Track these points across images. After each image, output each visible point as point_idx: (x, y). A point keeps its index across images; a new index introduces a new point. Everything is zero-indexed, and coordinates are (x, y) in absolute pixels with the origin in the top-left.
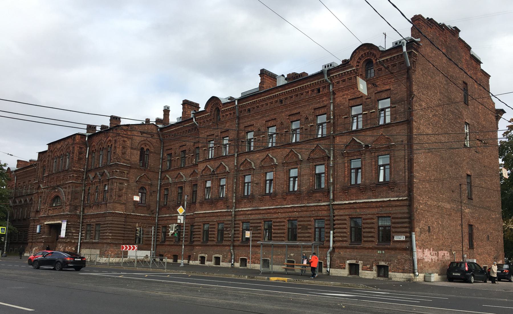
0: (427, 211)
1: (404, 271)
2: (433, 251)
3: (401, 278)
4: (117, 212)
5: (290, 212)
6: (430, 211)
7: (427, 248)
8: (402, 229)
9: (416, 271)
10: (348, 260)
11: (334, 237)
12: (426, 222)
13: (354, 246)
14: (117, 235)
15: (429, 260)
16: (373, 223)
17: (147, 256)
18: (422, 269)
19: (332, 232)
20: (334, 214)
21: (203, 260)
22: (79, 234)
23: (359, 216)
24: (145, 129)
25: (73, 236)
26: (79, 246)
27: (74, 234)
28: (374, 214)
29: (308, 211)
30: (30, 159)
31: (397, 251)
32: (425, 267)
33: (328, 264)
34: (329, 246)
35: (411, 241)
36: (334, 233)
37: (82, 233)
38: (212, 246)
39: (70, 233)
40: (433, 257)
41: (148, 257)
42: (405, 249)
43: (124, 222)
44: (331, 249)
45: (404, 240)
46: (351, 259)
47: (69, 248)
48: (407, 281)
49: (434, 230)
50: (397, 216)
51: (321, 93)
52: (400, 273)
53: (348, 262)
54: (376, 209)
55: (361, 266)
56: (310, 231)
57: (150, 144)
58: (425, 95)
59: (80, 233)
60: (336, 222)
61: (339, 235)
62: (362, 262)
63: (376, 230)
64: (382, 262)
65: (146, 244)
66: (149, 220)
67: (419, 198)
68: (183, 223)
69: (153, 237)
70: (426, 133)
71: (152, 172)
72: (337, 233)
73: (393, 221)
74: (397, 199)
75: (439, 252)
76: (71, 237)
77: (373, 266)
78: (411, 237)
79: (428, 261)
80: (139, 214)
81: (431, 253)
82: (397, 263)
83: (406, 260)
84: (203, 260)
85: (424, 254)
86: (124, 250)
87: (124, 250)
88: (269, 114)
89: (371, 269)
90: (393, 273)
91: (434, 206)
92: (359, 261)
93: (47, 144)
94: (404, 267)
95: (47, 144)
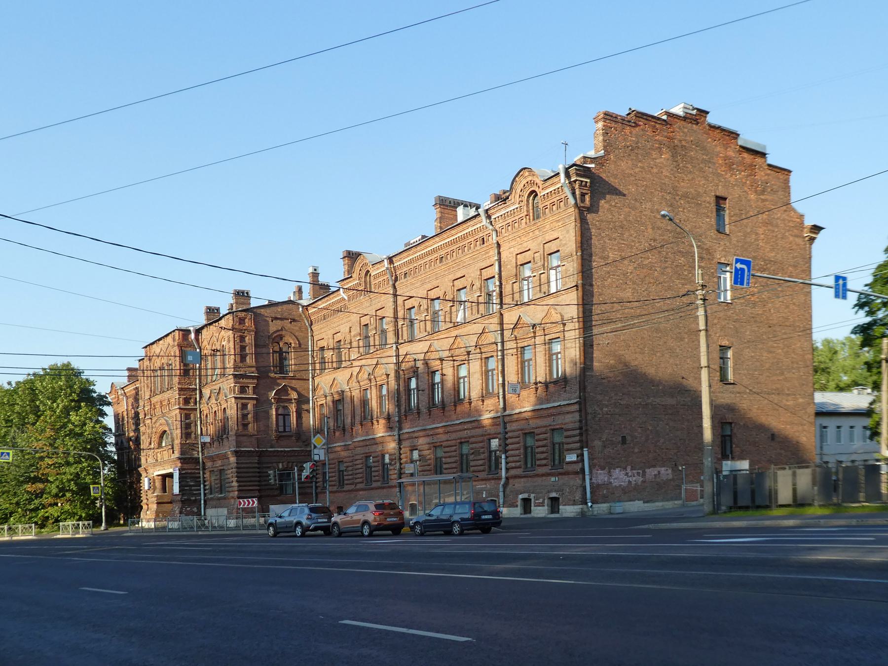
1: (574, 503)
4: (242, 449)
5: (460, 430)
9: (588, 501)
11: (507, 463)
14: (248, 484)
16: (545, 439)
18: (607, 497)
19: (503, 456)
25: (191, 490)
26: (202, 505)
27: (193, 488)
30: (604, 110)
33: (501, 501)
35: (583, 461)
36: (507, 457)
37: (205, 486)
38: (376, 489)
42: (577, 473)
43: (258, 463)
44: (503, 480)
47: (189, 509)
51: (485, 244)
53: (521, 496)
55: (533, 500)
56: (482, 456)
58: (615, 239)
59: (202, 486)
60: (509, 441)
68: (323, 459)
70: (617, 298)
72: (510, 456)
75: (648, 470)
76: (188, 492)
78: (582, 455)
80: (282, 449)
86: (241, 506)
87: (241, 506)
93: (143, 348)
95: (143, 348)
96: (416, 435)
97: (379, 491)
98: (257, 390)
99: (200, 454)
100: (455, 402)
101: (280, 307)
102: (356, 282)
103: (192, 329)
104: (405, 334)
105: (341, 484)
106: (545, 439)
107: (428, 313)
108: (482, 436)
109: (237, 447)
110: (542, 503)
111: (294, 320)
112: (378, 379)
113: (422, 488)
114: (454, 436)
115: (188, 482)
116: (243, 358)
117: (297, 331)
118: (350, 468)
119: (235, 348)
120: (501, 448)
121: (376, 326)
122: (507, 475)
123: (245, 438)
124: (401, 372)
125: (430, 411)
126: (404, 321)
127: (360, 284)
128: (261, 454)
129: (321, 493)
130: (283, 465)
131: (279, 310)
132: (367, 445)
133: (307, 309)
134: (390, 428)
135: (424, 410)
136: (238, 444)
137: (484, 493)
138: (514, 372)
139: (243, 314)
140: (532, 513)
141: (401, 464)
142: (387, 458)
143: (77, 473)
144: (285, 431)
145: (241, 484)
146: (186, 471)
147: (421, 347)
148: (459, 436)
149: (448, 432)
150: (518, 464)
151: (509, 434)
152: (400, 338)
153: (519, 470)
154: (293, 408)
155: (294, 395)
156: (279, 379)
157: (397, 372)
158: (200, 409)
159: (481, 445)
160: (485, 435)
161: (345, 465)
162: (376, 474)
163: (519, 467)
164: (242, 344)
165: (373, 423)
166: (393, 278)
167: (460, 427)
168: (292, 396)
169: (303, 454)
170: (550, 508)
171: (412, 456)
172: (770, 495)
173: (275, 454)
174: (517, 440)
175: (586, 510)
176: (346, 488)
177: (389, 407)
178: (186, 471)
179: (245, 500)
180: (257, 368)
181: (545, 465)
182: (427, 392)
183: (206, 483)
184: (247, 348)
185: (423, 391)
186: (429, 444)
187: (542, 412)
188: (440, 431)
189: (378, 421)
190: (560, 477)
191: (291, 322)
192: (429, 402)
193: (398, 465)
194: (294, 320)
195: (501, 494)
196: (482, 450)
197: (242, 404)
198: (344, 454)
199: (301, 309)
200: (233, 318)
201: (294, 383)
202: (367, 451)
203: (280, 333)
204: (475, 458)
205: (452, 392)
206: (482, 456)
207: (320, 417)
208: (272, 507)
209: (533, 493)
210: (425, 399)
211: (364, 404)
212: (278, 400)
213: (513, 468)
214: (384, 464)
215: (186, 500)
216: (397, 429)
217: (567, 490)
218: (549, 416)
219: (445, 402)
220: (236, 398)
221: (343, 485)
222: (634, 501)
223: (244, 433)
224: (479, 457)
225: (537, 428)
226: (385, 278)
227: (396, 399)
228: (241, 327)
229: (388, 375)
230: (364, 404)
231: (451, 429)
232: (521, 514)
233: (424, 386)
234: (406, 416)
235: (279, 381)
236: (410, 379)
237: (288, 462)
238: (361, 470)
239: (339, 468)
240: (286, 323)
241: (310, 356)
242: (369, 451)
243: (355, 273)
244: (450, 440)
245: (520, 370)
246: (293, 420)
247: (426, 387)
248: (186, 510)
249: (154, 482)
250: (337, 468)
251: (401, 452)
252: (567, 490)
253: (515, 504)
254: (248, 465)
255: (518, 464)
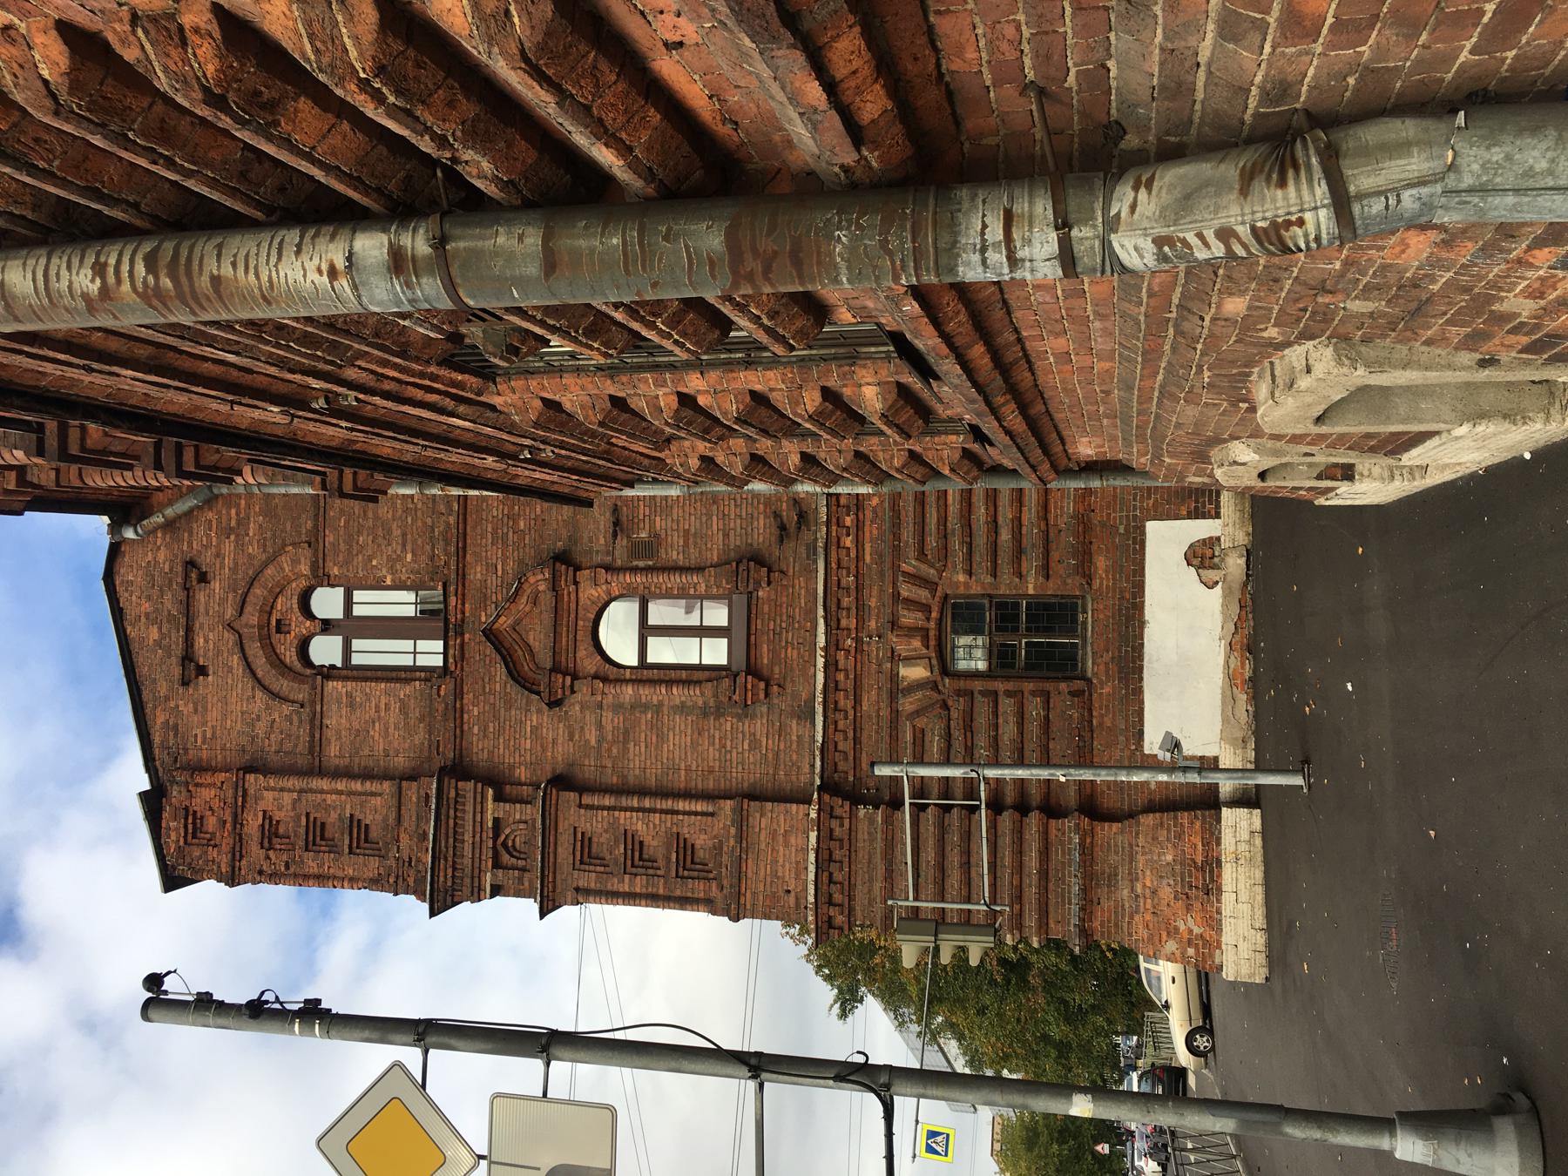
17: (1202, 557)
24: (158, 643)
41: (1212, 542)
57: (258, 591)
65: (1084, 556)
66: (859, 558)
69: (991, 773)
71: (461, 552)
80: (820, 662)
117: (240, 546)
130: (910, 660)
131: (154, 634)
143: (1070, 1071)
169: (848, 541)
172: (1513, 237)
237: (894, 624)
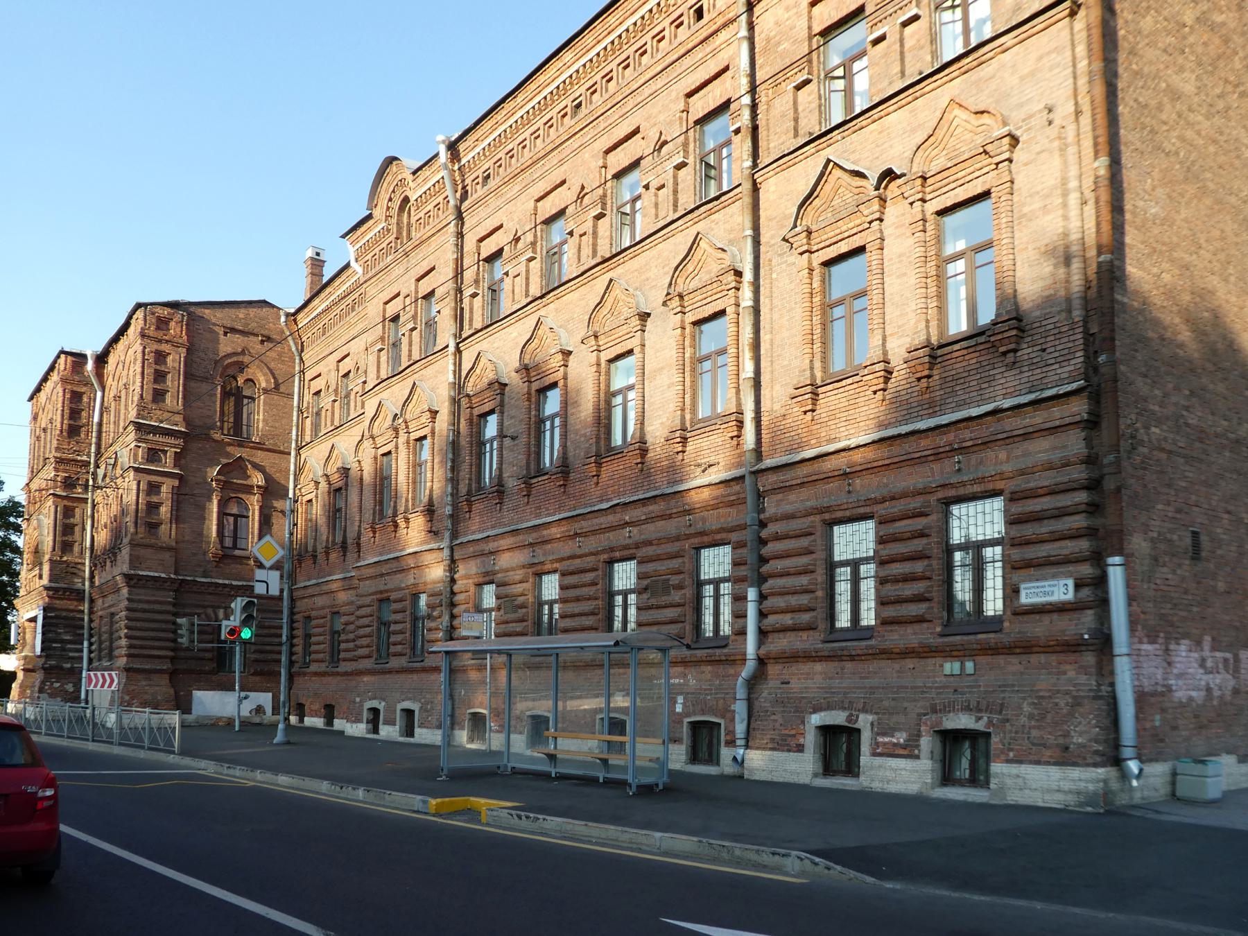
0: (1185, 457)
1: (1065, 757)
2: (1213, 649)
3: (1049, 791)
4: (141, 573)
5: (611, 528)
6: (1201, 461)
7: (1186, 636)
8: (1058, 544)
9: (1127, 752)
10: (816, 710)
11: (762, 615)
12: (1179, 511)
13: (842, 649)
15: (1194, 694)
16: (922, 534)
17: (259, 710)
18: (1162, 741)
20: (762, 516)
21: (374, 719)
22: (82, 644)
23: (862, 510)
27: (69, 646)
28: (925, 492)
29: (670, 516)
31: (1034, 658)
32: (1175, 728)
33: (740, 729)
34: (745, 654)
35: (1103, 603)
36: (762, 597)
37: (91, 644)
39: (56, 642)
40: (1216, 680)
42: (1072, 647)
43: (174, 605)
44: (751, 665)
45: (1069, 603)
46: (829, 707)
47: (57, 685)
48: (1081, 804)
49: (1219, 552)
50: (1032, 485)
52: (1048, 763)
53: (816, 719)
54: (936, 467)
55: (866, 737)
56: (676, 596)
59: (86, 644)
61: (779, 602)
62: (870, 718)
63: (934, 563)
64: (961, 715)
67: (1141, 385)
72: (773, 594)
73: (1017, 508)
74: (1032, 397)
77: (919, 735)
78: (1101, 581)
79: (1191, 699)
80: (227, 582)
81: (1203, 660)
82: (1031, 717)
83: (1077, 703)
84: (374, 719)
85: (1169, 664)
88: (546, 169)
89: (909, 751)
90: (1014, 769)
91: (1217, 436)
92: (862, 717)
94: (1066, 735)
96: (492, 546)
97: (402, 677)
98: (183, 462)
99: (87, 583)
100: (598, 455)
101: (243, 310)
102: (381, 226)
103: (89, 353)
104: (477, 312)
105: (336, 659)
106: (922, 534)
107: (534, 251)
108: (678, 538)
109: (132, 566)
110: (904, 747)
111: (268, 339)
112: (412, 426)
113: (503, 675)
114: (592, 544)
115: (60, 633)
116: (159, 396)
118: (351, 627)
119: (143, 373)
120: (743, 571)
121: (416, 313)
122: (762, 651)
123: (149, 551)
124: (464, 401)
125: (529, 486)
126: (477, 287)
127: (388, 231)
128: (180, 587)
129: (299, 674)
131: (241, 316)
132: (382, 575)
133: (295, 320)
134: (433, 533)
135: (511, 483)
136: (134, 561)
137: (680, 699)
138: (799, 338)
139: (166, 312)
140: (862, 778)
141: (453, 617)
142: (423, 600)
144: (235, 547)
145: (135, 642)
146: (58, 613)
147: (516, 333)
148: (606, 544)
149: (576, 534)
150: (805, 617)
151: (772, 528)
152: (466, 326)
153: (804, 635)
154: (254, 503)
155: (258, 479)
156: (229, 444)
157: (455, 402)
158: (94, 501)
159: (675, 564)
160: (688, 536)
161: (344, 619)
162: (399, 638)
163: (810, 627)
164: (158, 367)
165: (396, 526)
166: (458, 195)
167: (611, 519)
168: (255, 480)
170: (938, 766)
171: (481, 599)
173: (211, 589)
174: (804, 542)
175: (1115, 785)
176: (344, 667)
177: (435, 481)
178: (58, 613)
179: (99, 674)
180: (186, 420)
181: (920, 620)
182: (523, 439)
183: (93, 640)
184: (169, 376)
185: (513, 438)
186: (524, 567)
187: (909, 446)
188: (555, 531)
189: (407, 520)
190: (982, 659)
191: (262, 342)
192: (528, 464)
193: (446, 618)
194: (268, 339)
195: (740, 708)
196: (675, 580)
197: (150, 483)
198: (342, 597)
199: (283, 319)
200: (145, 317)
201: (260, 457)
202: (382, 588)
203: (240, 358)
204: (653, 601)
205: (589, 431)
206: (676, 596)
207: (306, 525)
208: (198, 694)
209: (865, 710)
210: (517, 458)
211: (382, 485)
212: (226, 486)
213: (785, 630)
214: (415, 619)
215: (52, 667)
216: (447, 534)
217: (1026, 708)
218: (937, 456)
219: (571, 459)
220: (137, 470)
221: (339, 660)
222: (1219, 755)
223: (147, 541)
224: (665, 600)
225: (883, 500)
226: (440, 199)
227: (449, 464)
228: (160, 334)
229: (434, 413)
230: (382, 485)
231: (585, 525)
232: (815, 775)
233: (517, 422)
234: (470, 504)
235: (229, 449)
236: (485, 415)
238: (368, 630)
239: (332, 626)
240: (254, 344)
241: (296, 409)
242: (386, 588)
243: (379, 207)
244: (580, 557)
245: (818, 331)
246: (253, 528)
247: (522, 428)
248: (51, 687)
249: (24, 633)
250: (328, 625)
251: (456, 588)
252: (1026, 708)
253: (793, 743)
254: (146, 606)
255: (805, 617)
